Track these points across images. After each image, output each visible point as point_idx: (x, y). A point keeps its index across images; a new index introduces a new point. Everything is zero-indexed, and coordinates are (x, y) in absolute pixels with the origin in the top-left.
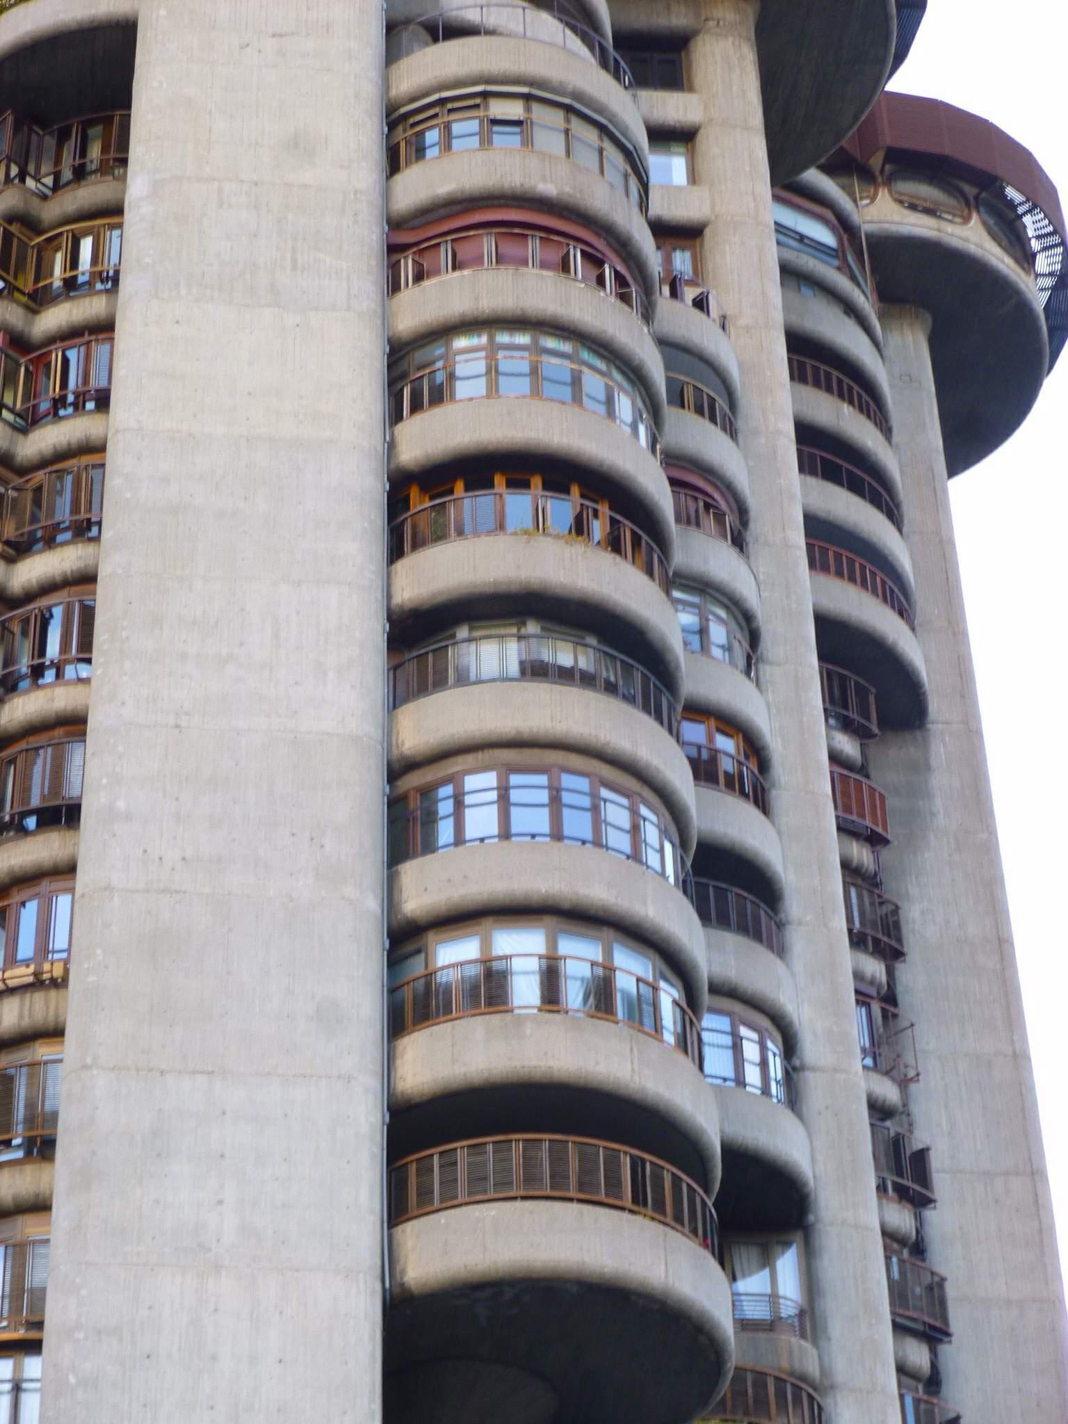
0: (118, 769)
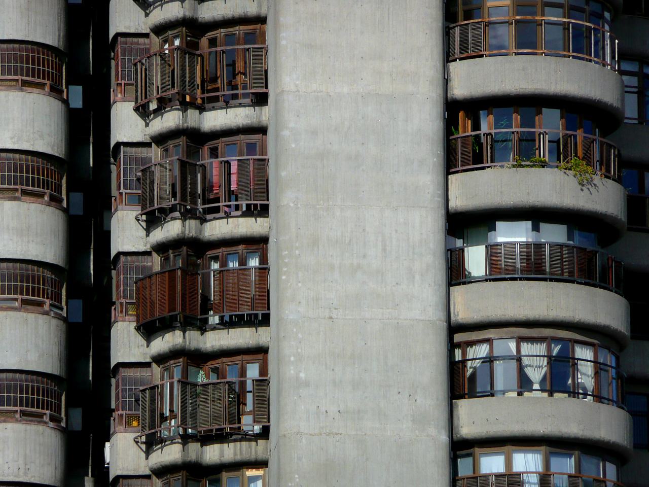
0: (299, 350)
